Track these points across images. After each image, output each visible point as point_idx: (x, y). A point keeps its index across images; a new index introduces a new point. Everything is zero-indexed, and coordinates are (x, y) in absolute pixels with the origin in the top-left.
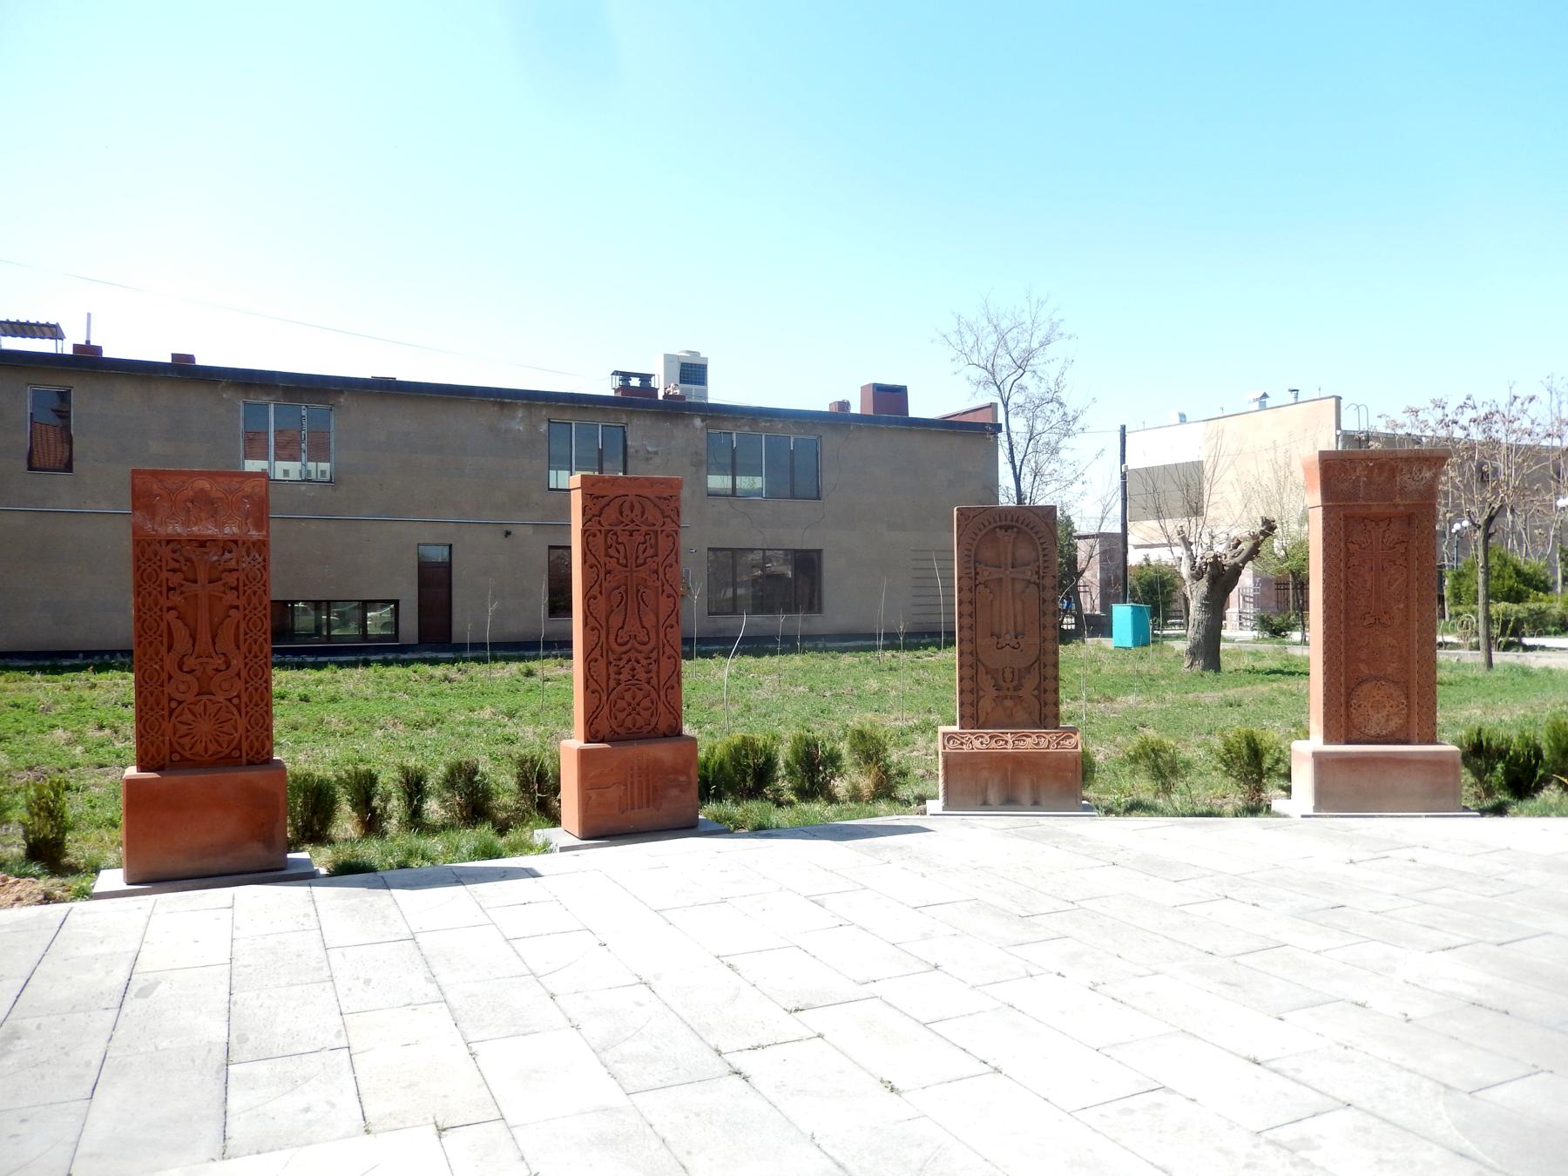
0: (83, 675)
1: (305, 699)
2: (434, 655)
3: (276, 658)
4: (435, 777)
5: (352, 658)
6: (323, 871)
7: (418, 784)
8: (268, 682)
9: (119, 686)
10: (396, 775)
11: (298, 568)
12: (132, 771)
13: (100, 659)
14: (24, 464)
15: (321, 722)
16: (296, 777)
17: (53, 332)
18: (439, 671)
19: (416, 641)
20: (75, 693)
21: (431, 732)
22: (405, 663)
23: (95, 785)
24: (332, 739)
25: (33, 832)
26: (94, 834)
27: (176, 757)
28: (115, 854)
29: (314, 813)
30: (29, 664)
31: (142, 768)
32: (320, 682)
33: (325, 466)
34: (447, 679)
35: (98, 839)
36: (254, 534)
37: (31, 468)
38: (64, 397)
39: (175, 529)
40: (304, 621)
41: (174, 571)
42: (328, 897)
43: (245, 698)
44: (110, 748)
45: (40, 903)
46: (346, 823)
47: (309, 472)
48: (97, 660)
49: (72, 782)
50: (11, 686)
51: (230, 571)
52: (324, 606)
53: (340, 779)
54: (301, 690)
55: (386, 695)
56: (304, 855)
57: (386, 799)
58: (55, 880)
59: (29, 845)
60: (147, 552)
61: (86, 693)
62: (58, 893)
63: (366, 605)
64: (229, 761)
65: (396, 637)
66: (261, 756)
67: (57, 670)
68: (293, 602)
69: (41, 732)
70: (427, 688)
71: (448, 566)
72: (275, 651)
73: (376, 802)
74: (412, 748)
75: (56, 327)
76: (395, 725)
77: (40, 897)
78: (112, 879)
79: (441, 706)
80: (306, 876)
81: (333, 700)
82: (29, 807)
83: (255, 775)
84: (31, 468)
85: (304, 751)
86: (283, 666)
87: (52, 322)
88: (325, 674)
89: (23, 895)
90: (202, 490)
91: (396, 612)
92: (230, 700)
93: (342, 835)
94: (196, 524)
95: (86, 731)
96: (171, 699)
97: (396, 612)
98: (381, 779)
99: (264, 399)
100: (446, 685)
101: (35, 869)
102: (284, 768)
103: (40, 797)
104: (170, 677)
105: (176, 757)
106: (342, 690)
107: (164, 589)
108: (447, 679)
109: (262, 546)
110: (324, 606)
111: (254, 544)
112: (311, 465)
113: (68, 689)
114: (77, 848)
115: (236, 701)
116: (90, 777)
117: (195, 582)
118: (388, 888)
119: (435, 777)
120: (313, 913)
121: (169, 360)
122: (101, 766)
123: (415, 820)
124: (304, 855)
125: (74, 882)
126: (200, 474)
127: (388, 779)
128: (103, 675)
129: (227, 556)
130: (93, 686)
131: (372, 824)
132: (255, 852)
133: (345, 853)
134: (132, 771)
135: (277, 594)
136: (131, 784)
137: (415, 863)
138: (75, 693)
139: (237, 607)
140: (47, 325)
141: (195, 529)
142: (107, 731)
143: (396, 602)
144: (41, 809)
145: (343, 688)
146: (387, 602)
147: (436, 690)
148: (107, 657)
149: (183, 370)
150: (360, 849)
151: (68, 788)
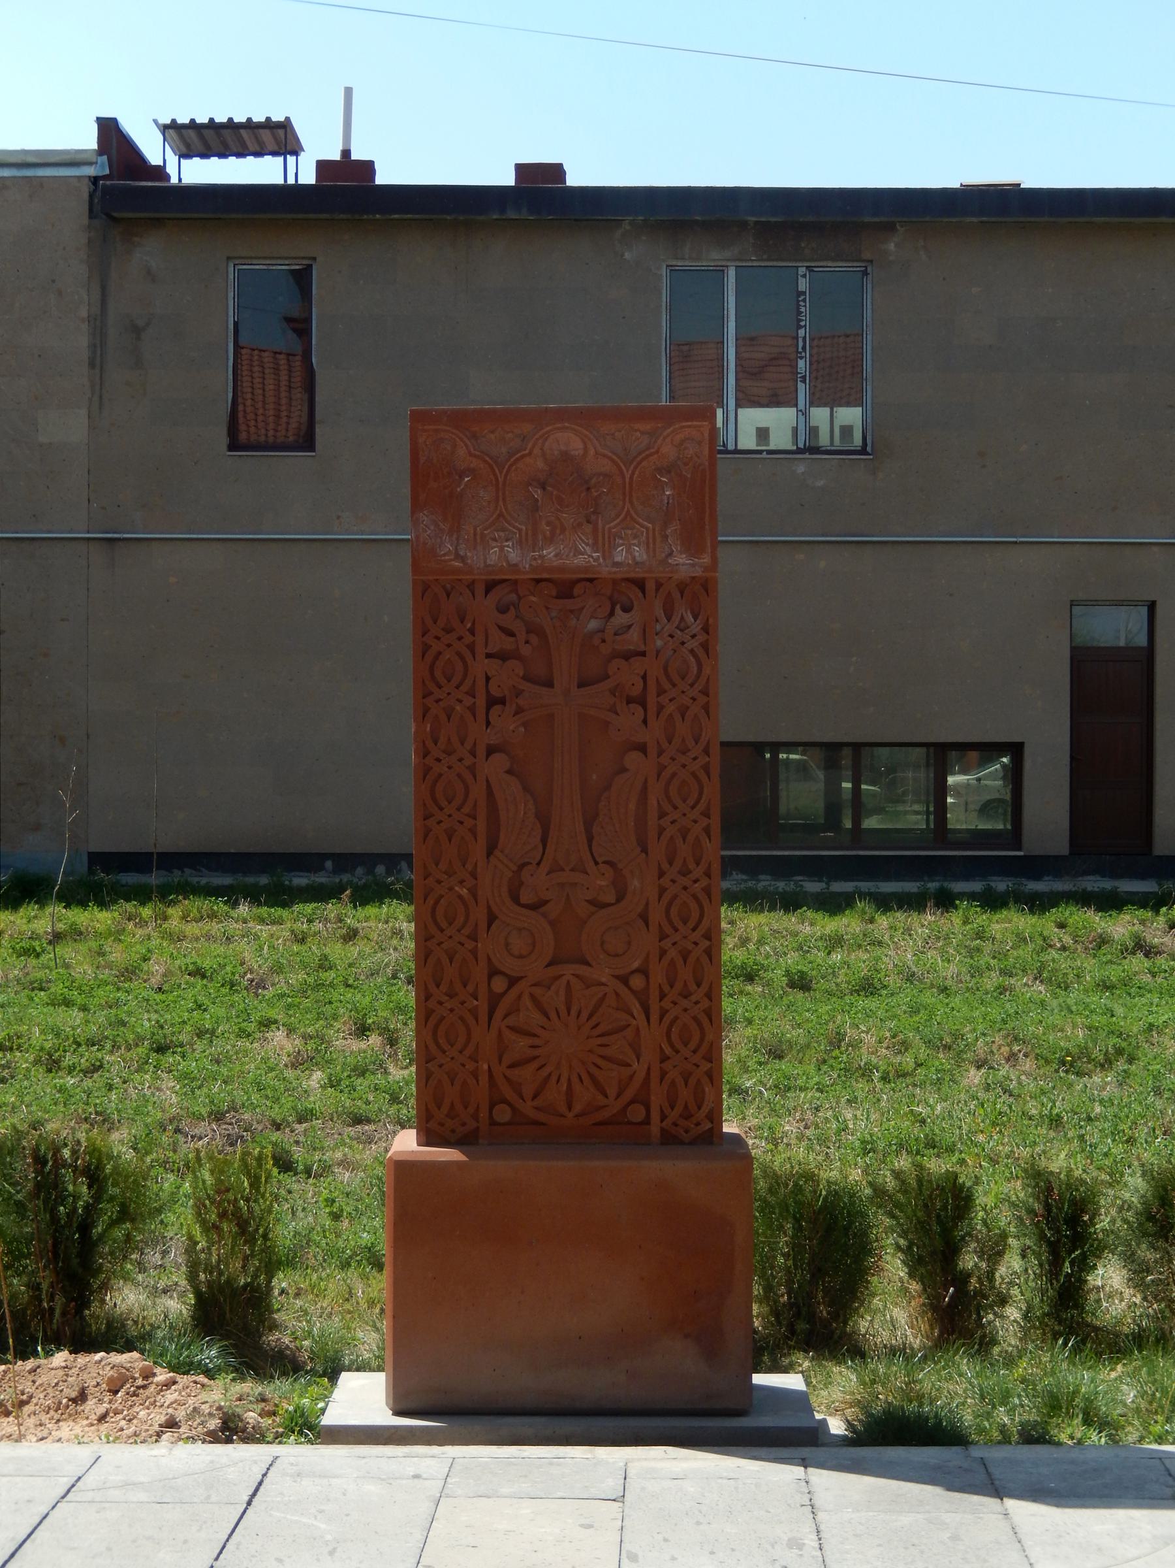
0: (332, 909)
1: (800, 983)
2: (1107, 884)
3: (735, 882)
4: (1120, 1200)
5: (911, 887)
6: (837, 1427)
7: (1074, 1221)
8: (713, 937)
9: (385, 934)
10: (1018, 1190)
11: (786, 659)
12: (406, 1142)
13: (360, 875)
14: (224, 440)
15: (837, 1040)
16: (776, 1181)
17: (277, 138)
18: (1121, 926)
19: (1065, 851)
20: (314, 949)
21: (1103, 1082)
22: (1038, 904)
23: (345, 1163)
24: (861, 1087)
25: (209, 1269)
26: (335, 1281)
27: (503, 1114)
28: (369, 1339)
29: (818, 1273)
30: (227, 880)
31: (428, 1137)
32: (835, 942)
33: (850, 415)
34: (1141, 947)
35: (332, 1298)
36: (683, 564)
37: (234, 446)
38: (302, 278)
39: (505, 554)
40: (802, 795)
41: (502, 656)
42: (848, 1497)
43: (658, 976)
44: (379, 1079)
45: (214, 1437)
46: (893, 1309)
47: (813, 431)
48: (360, 875)
49: (298, 1154)
50: (192, 929)
51: (627, 656)
52: (847, 754)
53: (879, 1192)
54: (792, 960)
55: (992, 981)
56: (792, 1381)
57: (994, 1252)
58: (248, 1387)
59: (199, 1295)
60: (441, 602)
61: (336, 951)
62: (251, 1417)
63: (943, 756)
64: (617, 1129)
65: (1015, 836)
66: (689, 1122)
67: (282, 897)
68: (776, 747)
69: (243, 1034)
70: (1093, 969)
71: (1143, 660)
72: (730, 865)
73: (969, 1260)
74: (1055, 1122)
75: (285, 126)
76: (1012, 1058)
77: (214, 1424)
78: (361, 1397)
79: (1130, 1015)
80: (788, 1437)
81: (867, 987)
82: (199, 1208)
83: (677, 1170)
84: (234, 446)
85: (796, 1122)
86: (753, 900)
87: (278, 117)
88: (848, 924)
89: (180, 1415)
90: (566, 457)
91: (1015, 776)
92: (624, 980)
93: (885, 1337)
94: (550, 540)
95: (273, 1045)
96: (493, 972)
97: (1015, 776)
98: (983, 1198)
99: (713, 256)
100: (1138, 962)
101: (210, 1354)
102: (747, 1158)
103: (222, 1189)
104: (492, 919)
105: (503, 1114)
106: (886, 963)
107: (481, 702)
108: (1141, 947)
109: (700, 592)
110: (847, 754)
111: (682, 587)
112: (820, 415)
113: (301, 939)
114: (301, 1311)
115: (637, 982)
116: (337, 1146)
117: (550, 684)
118: (998, 1492)
119: (1120, 1200)
120: (811, 1541)
121: (507, 178)
122: (358, 1120)
123: (1066, 1314)
124: (792, 1381)
125: (285, 1393)
126: (562, 415)
127: (999, 1198)
128: (371, 910)
129: (621, 618)
130: (351, 936)
131: (958, 1316)
132: (677, 1363)
133: (891, 1387)
134: (406, 1142)
135: (734, 724)
136: (404, 1169)
137: (1068, 1431)
138: (314, 949)
139: (642, 748)
140: (268, 125)
141: (549, 552)
142: (375, 1040)
143: (1016, 750)
144: (223, 1215)
145: (888, 959)
146: (988, 750)
147: (1114, 973)
148: (380, 869)
149: (540, 198)
150: (928, 1379)
151: (285, 1165)
